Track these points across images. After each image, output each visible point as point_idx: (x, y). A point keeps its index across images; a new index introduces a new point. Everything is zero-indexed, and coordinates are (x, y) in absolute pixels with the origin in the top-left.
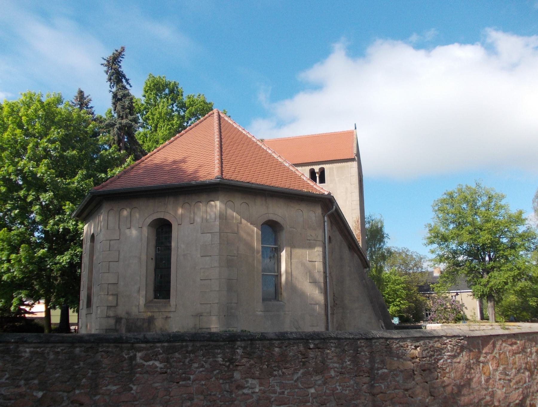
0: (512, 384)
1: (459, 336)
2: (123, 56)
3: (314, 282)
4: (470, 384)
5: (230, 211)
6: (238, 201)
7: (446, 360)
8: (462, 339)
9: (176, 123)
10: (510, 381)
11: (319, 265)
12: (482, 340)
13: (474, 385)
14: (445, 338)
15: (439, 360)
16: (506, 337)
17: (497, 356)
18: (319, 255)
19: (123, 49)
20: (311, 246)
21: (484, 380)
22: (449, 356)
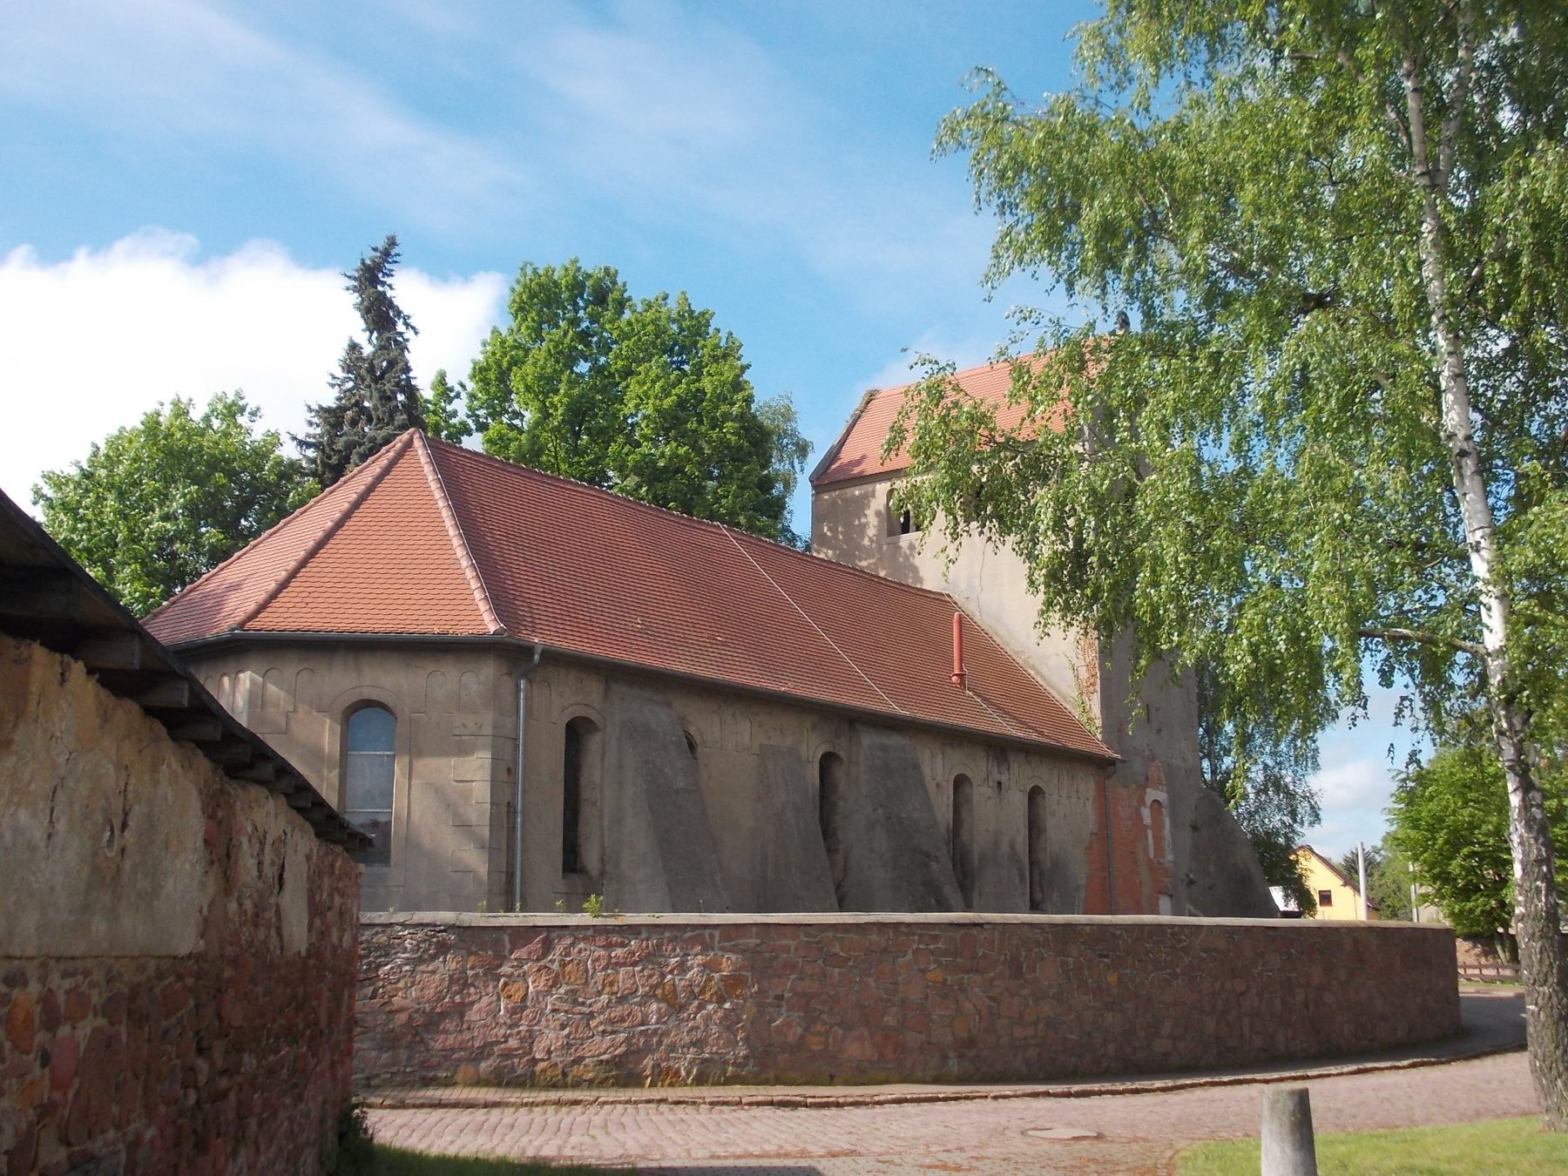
0: (593, 1023)
1: (436, 926)
2: (397, 259)
3: (464, 826)
4: (462, 1015)
5: (272, 689)
6: (291, 667)
7: (400, 966)
8: (440, 931)
9: (560, 401)
10: (591, 1015)
11: (481, 791)
12: (510, 935)
13: (472, 1015)
14: (399, 928)
15: (380, 965)
16: (590, 933)
17: (555, 966)
18: (482, 766)
19: (392, 242)
20: (463, 750)
21: (506, 1008)
22: (408, 959)
